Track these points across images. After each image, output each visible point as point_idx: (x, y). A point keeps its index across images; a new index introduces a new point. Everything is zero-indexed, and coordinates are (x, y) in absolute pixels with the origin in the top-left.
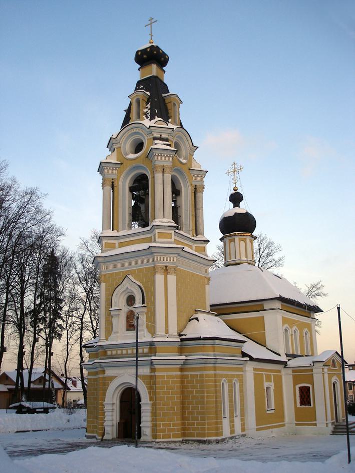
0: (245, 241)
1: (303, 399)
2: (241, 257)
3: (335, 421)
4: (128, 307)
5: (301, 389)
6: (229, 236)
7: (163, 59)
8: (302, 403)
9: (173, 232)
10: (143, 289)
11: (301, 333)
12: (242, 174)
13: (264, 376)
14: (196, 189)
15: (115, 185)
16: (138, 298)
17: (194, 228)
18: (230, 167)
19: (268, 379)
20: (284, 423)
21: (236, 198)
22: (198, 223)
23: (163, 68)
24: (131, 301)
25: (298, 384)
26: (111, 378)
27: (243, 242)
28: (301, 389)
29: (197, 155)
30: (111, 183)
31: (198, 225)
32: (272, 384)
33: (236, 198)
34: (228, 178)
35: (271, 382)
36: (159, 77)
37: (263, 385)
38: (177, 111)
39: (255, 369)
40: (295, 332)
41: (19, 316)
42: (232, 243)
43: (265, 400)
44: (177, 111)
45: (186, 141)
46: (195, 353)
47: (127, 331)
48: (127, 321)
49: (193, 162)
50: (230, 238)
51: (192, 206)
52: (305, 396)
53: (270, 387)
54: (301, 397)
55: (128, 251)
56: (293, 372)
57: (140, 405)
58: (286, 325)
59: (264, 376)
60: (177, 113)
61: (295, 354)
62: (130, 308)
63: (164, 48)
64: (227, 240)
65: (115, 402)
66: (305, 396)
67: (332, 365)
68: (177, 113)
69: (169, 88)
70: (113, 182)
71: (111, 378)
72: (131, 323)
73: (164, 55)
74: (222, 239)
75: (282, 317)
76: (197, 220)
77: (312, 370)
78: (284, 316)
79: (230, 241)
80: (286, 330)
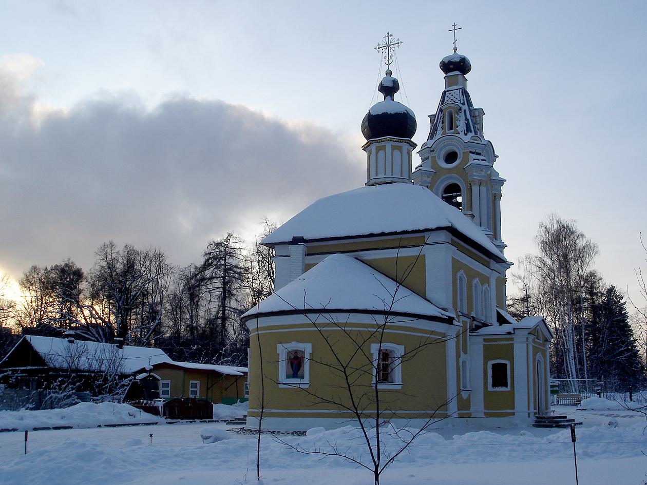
0: (400, 149)
2: (394, 173)
5: (494, 366)
6: (377, 142)
8: (494, 385)
12: (397, 52)
18: (382, 41)
20: (459, 412)
21: (389, 89)
25: (491, 360)
27: (397, 150)
33: (389, 89)
34: (380, 56)
41: (438, 419)
42: (381, 153)
50: (378, 145)
52: (500, 375)
55: (126, 428)
56: (485, 340)
59: (586, 376)
64: (373, 147)
66: (500, 375)
74: (365, 148)
75: (453, 259)
77: (512, 339)
78: (453, 256)
79: (378, 149)
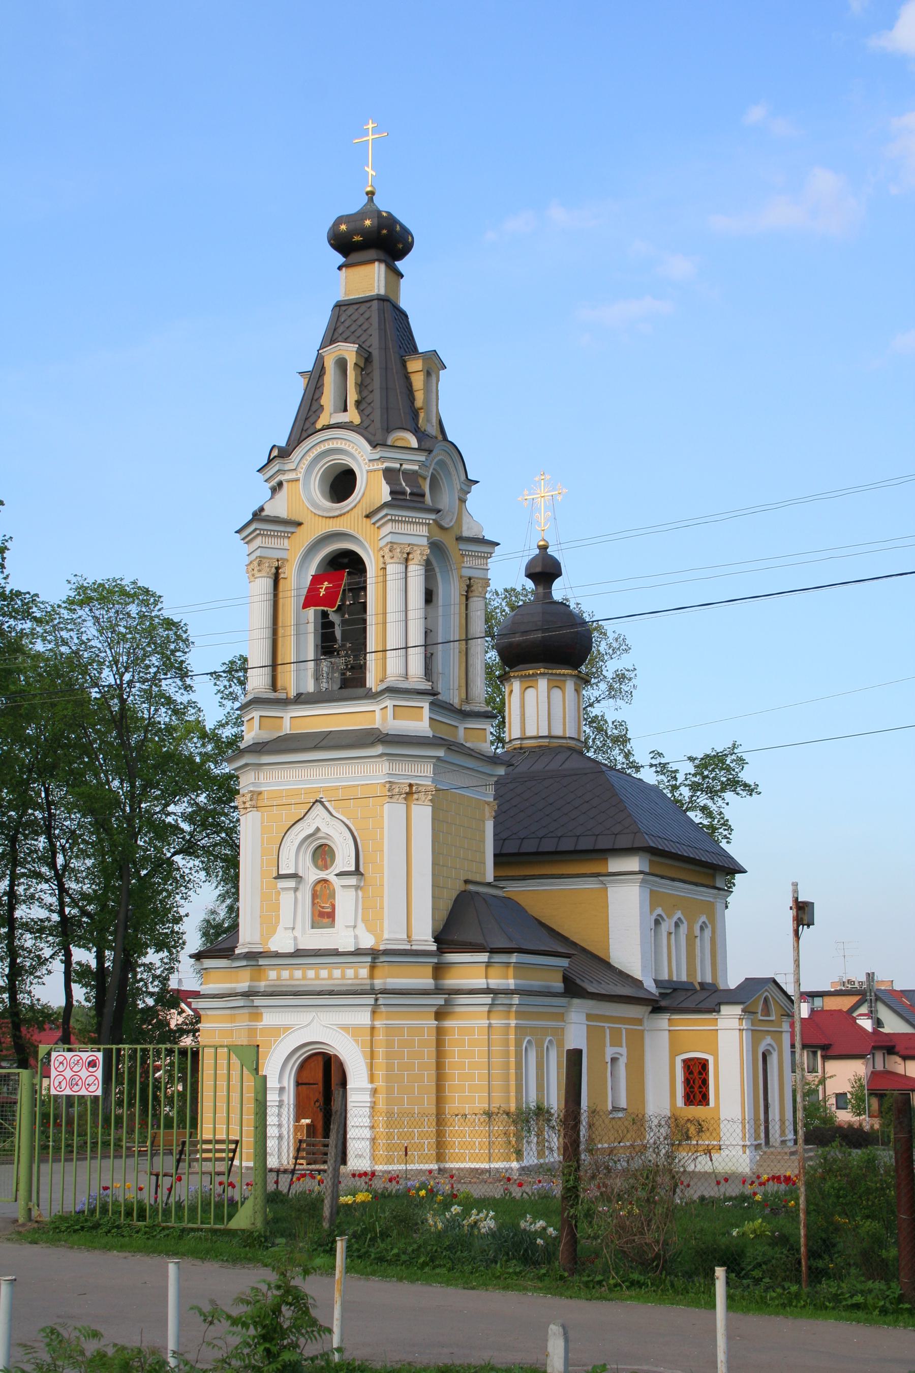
1: (692, 1087)
3: (763, 1141)
4: (319, 872)
7: (401, 246)
9: (426, 706)
10: (356, 834)
11: (690, 929)
13: (608, 1031)
14: (469, 586)
15: (282, 576)
16: (344, 860)
17: (464, 684)
19: (616, 1043)
22: (471, 669)
23: (398, 264)
24: (324, 859)
26: (278, 1031)
28: (687, 1063)
29: (474, 501)
30: (273, 570)
31: (470, 674)
32: (623, 1050)
35: (621, 1046)
36: (392, 297)
37: (603, 1054)
38: (434, 391)
39: (589, 1017)
40: (677, 925)
43: (606, 1088)
44: (434, 391)
45: (452, 469)
46: (360, 911)
47: (313, 928)
48: (313, 904)
49: (465, 519)
51: (460, 628)
53: (618, 1059)
54: (688, 1082)
57: (104, 1001)
58: (659, 911)
59: (608, 1031)
60: (434, 400)
61: (675, 979)
62: (322, 875)
63: (407, 217)
65: (285, 1084)
67: (762, 1010)
68: (434, 400)
69: (410, 320)
70: (277, 568)
71: (278, 1031)
72: (323, 907)
73: (406, 232)
76: (470, 662)
80: (657, 922)
